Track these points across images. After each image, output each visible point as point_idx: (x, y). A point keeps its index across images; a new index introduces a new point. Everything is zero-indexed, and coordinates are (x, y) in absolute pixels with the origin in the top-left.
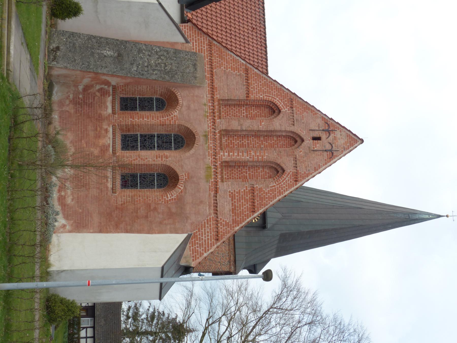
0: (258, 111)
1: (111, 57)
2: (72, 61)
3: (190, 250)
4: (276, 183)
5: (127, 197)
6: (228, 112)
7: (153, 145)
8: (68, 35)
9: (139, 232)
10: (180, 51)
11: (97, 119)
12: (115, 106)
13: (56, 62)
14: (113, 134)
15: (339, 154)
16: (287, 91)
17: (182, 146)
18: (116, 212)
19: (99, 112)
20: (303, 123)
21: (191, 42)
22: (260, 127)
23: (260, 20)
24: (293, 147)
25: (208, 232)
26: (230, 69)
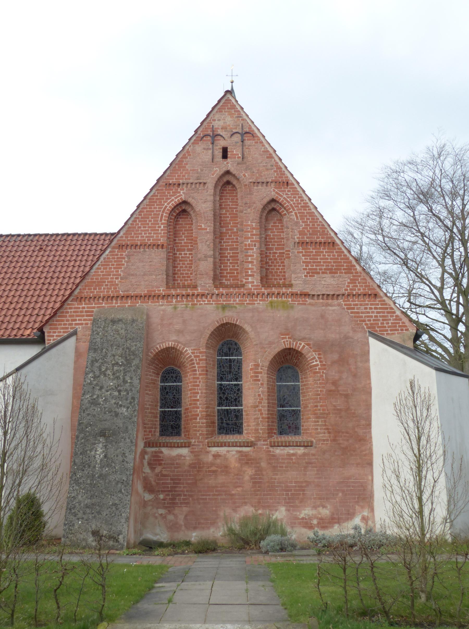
0: (183, 234)
1: (105, 448)
2: (117, 509)
3: (392, 334)
4: (292, 212)
5: (318, 425)
6: (184, 277)
7: (234, 387)
8: (71, 517)
9: (369, 407)
10: (91, 342)
11: (198, 471)
12: (178, 443)
13: (118, 535)
14: (222, 446)
15: (248, 125)
16: (154, 191)
17: (236, 344)
18: (341, 442)
19: (186, 468)
20: (202, 170)
21: (75, 327)
22: (208, 230)
23: (27, 241)
24: (237, 186)
25: (366, 308)
26: (120, 270)
